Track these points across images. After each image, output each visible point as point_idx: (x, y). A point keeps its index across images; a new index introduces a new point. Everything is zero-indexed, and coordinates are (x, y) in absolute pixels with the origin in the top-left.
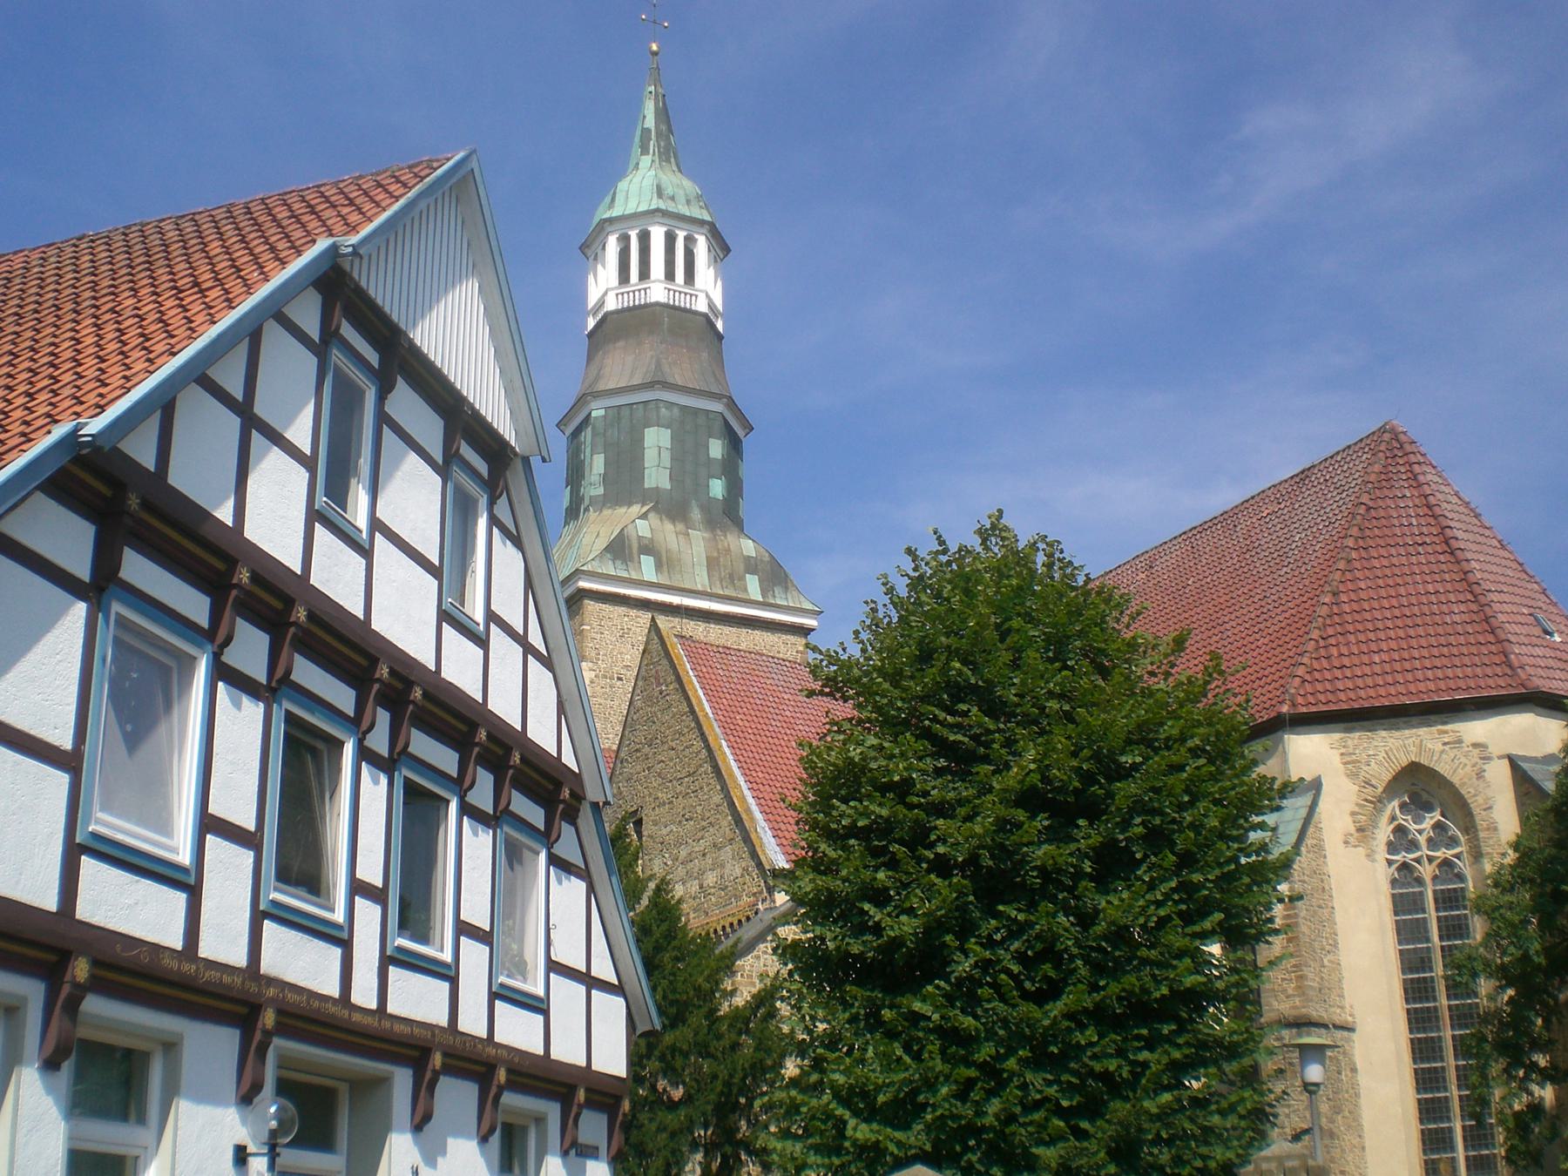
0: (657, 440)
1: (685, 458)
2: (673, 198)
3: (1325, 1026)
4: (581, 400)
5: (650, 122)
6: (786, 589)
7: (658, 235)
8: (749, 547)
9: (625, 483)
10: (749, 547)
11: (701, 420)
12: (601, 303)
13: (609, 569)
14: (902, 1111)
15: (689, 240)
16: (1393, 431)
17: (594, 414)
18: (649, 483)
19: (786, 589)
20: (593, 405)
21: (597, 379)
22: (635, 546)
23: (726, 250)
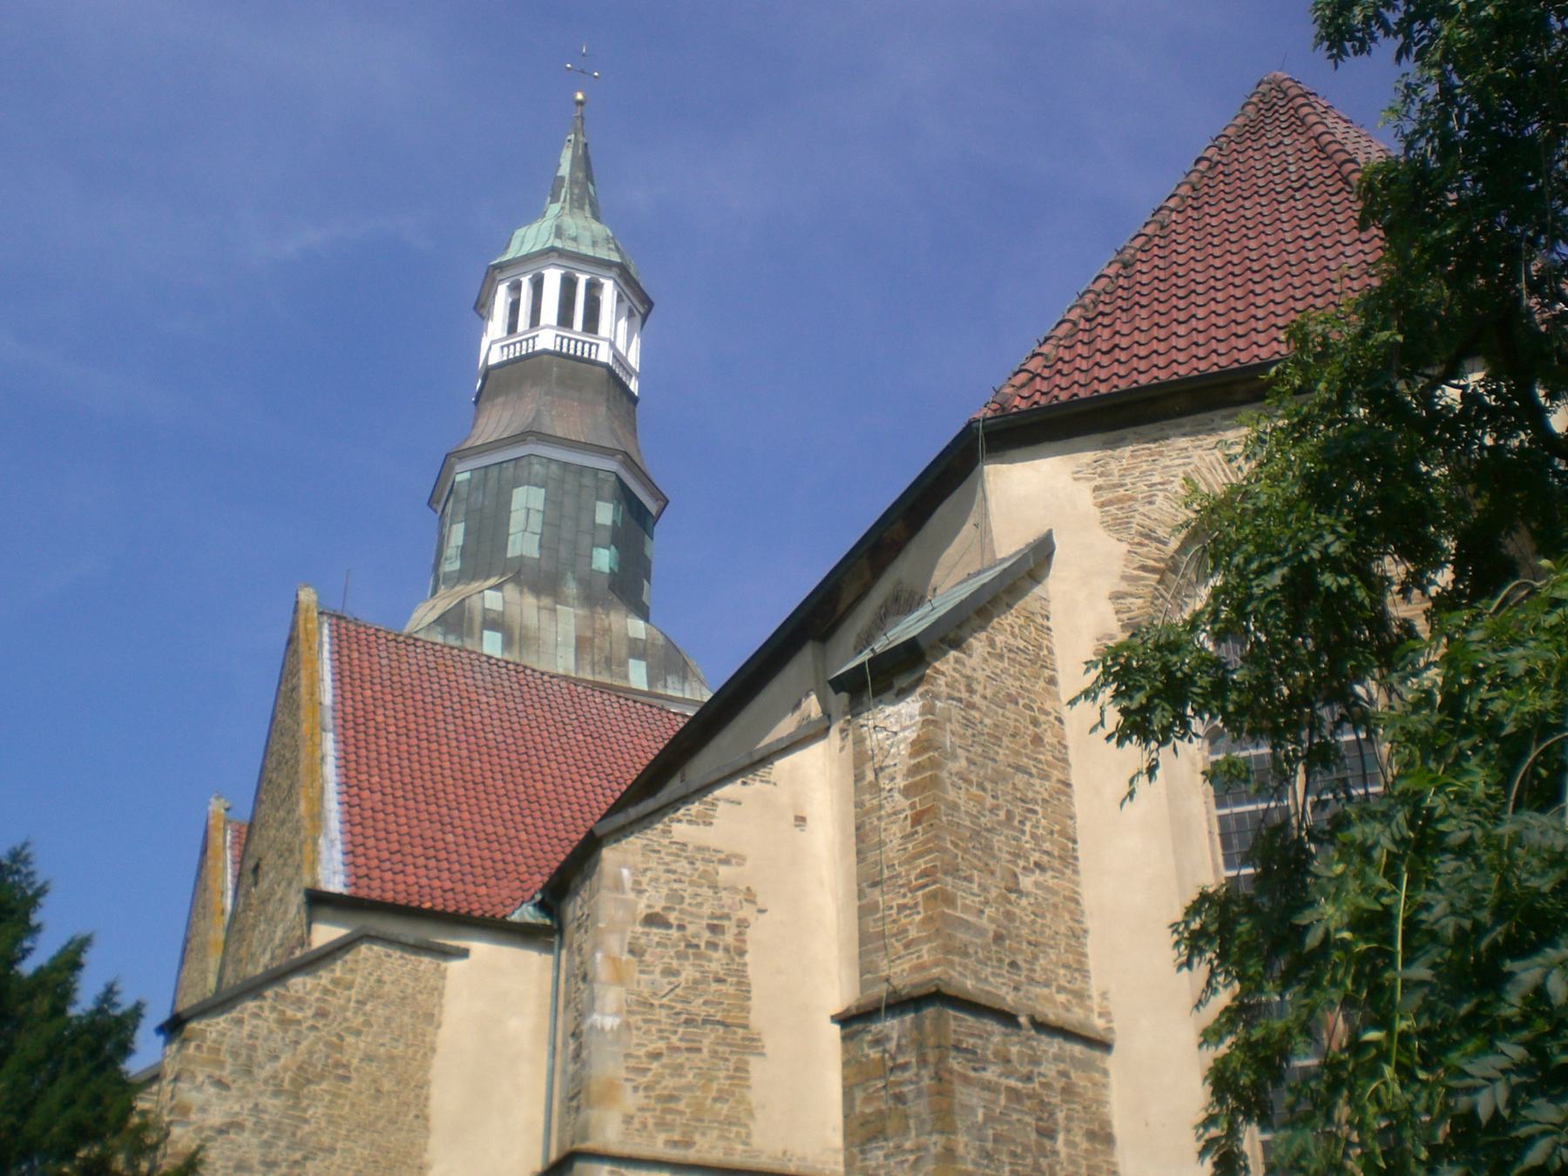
0: (527, 502)
1: (560, 526)
2: (575, 239)
3: (1007, 1018)
5: (565, 170)
6: (684, 679)
8: (637, 628)
11: (588, 480)
16: (1278, 86)
17: (459, 478)
18: (513, 551)
19: (684, 679)
22: (478, 619)
23: (648, 303)
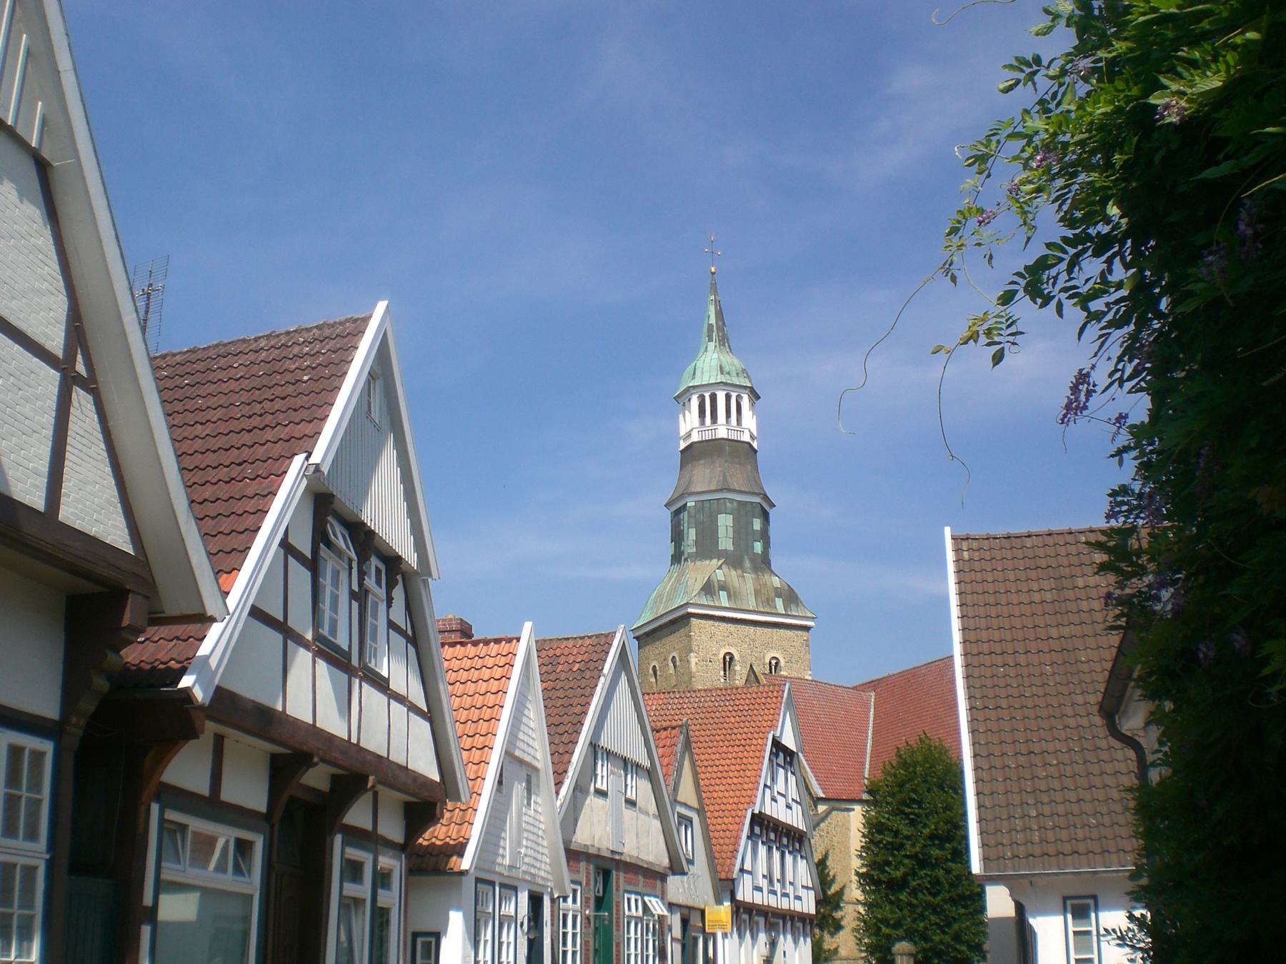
1: (742, 532)
4: (682, 496)
5: (713, 320)
7: (721, 397)
9: (708, 547)
10: (776, 582)
11: (749, 508)
12: (689, 435)
13: (704, 601)
14: (897, 925)
15: (739, 397)
20: (689, 499)
21: (690, 483)
23: (758, 397)
